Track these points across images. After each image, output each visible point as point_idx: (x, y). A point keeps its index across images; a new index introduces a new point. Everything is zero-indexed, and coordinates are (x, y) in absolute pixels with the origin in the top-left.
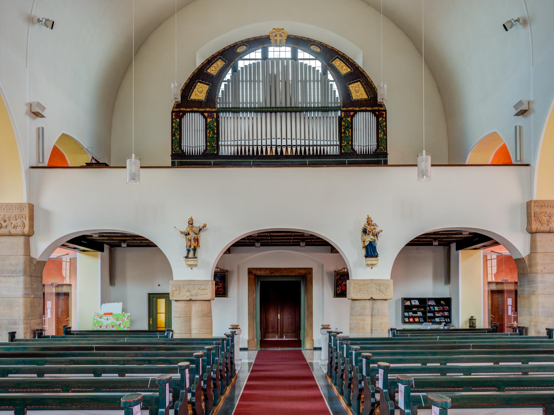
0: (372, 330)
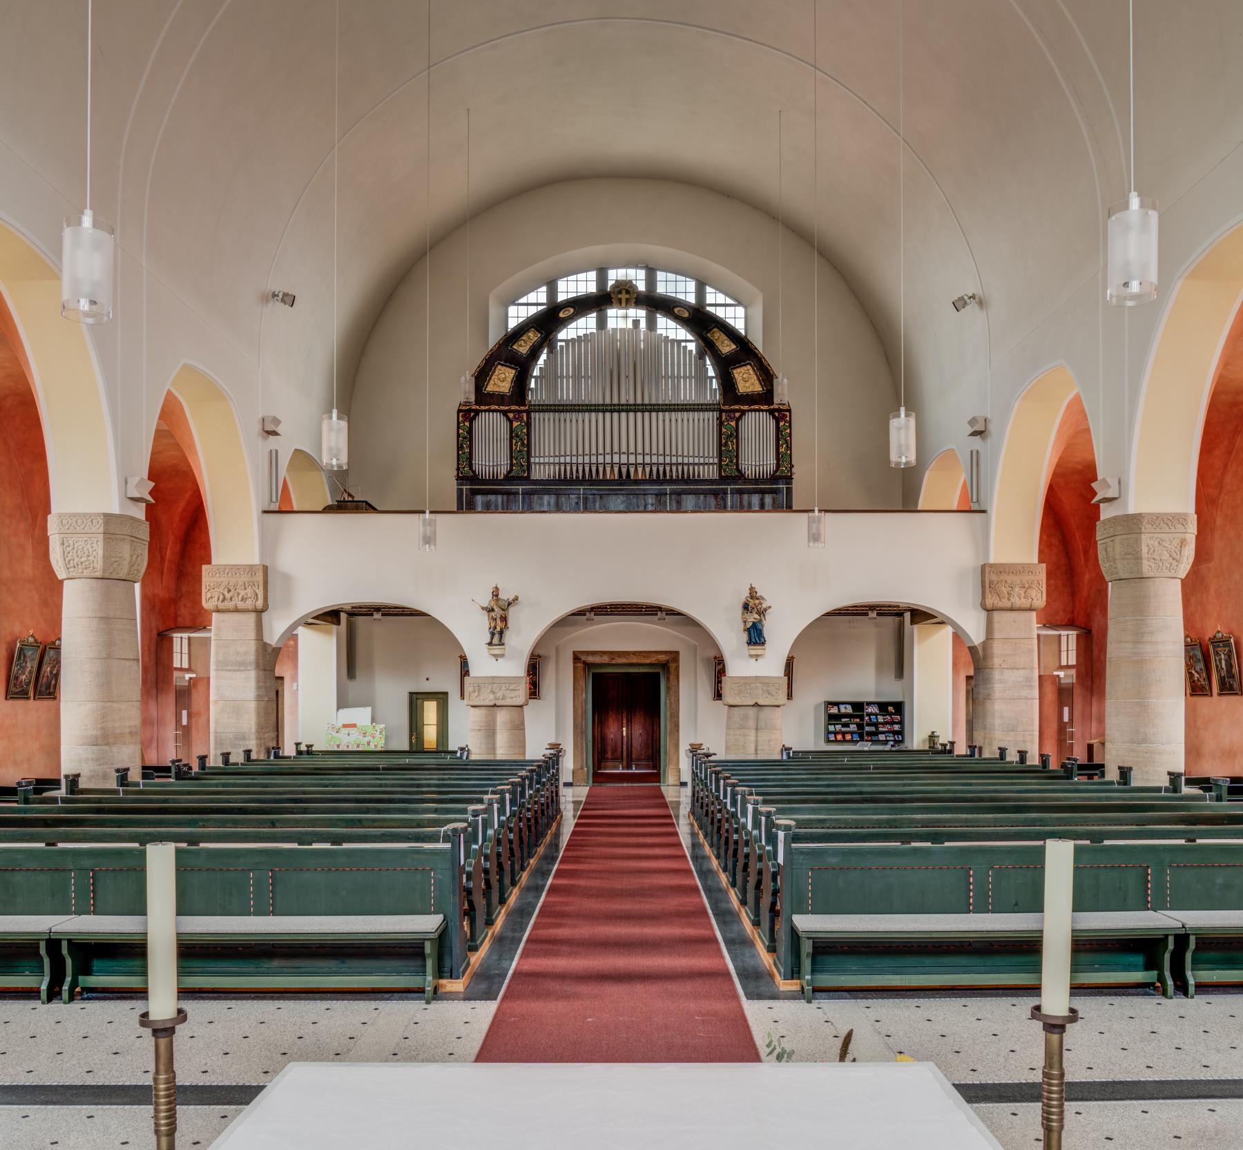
0: (756, 750)
